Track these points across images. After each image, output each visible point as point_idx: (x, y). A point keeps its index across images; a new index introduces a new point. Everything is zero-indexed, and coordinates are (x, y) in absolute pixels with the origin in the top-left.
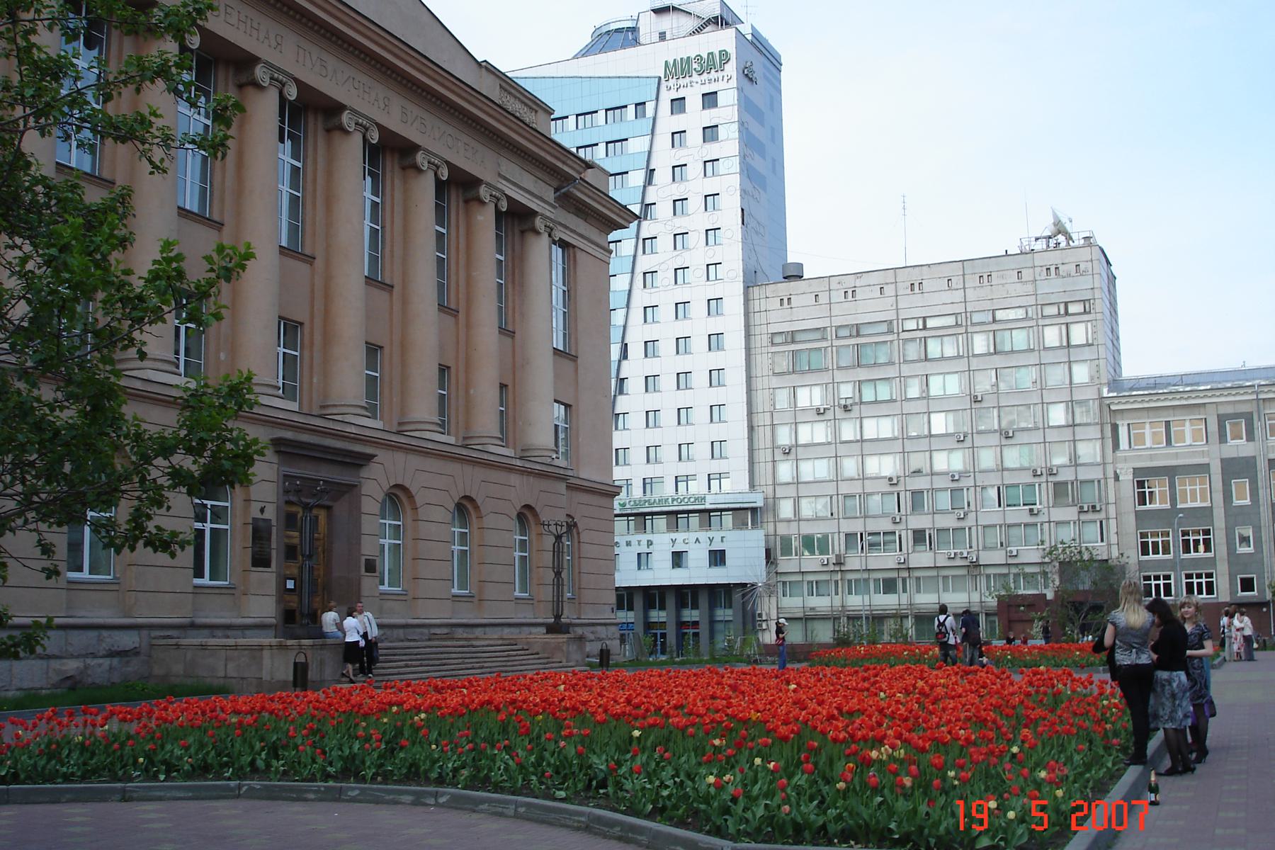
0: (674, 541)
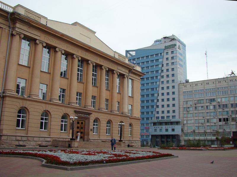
0: (166, 127)
